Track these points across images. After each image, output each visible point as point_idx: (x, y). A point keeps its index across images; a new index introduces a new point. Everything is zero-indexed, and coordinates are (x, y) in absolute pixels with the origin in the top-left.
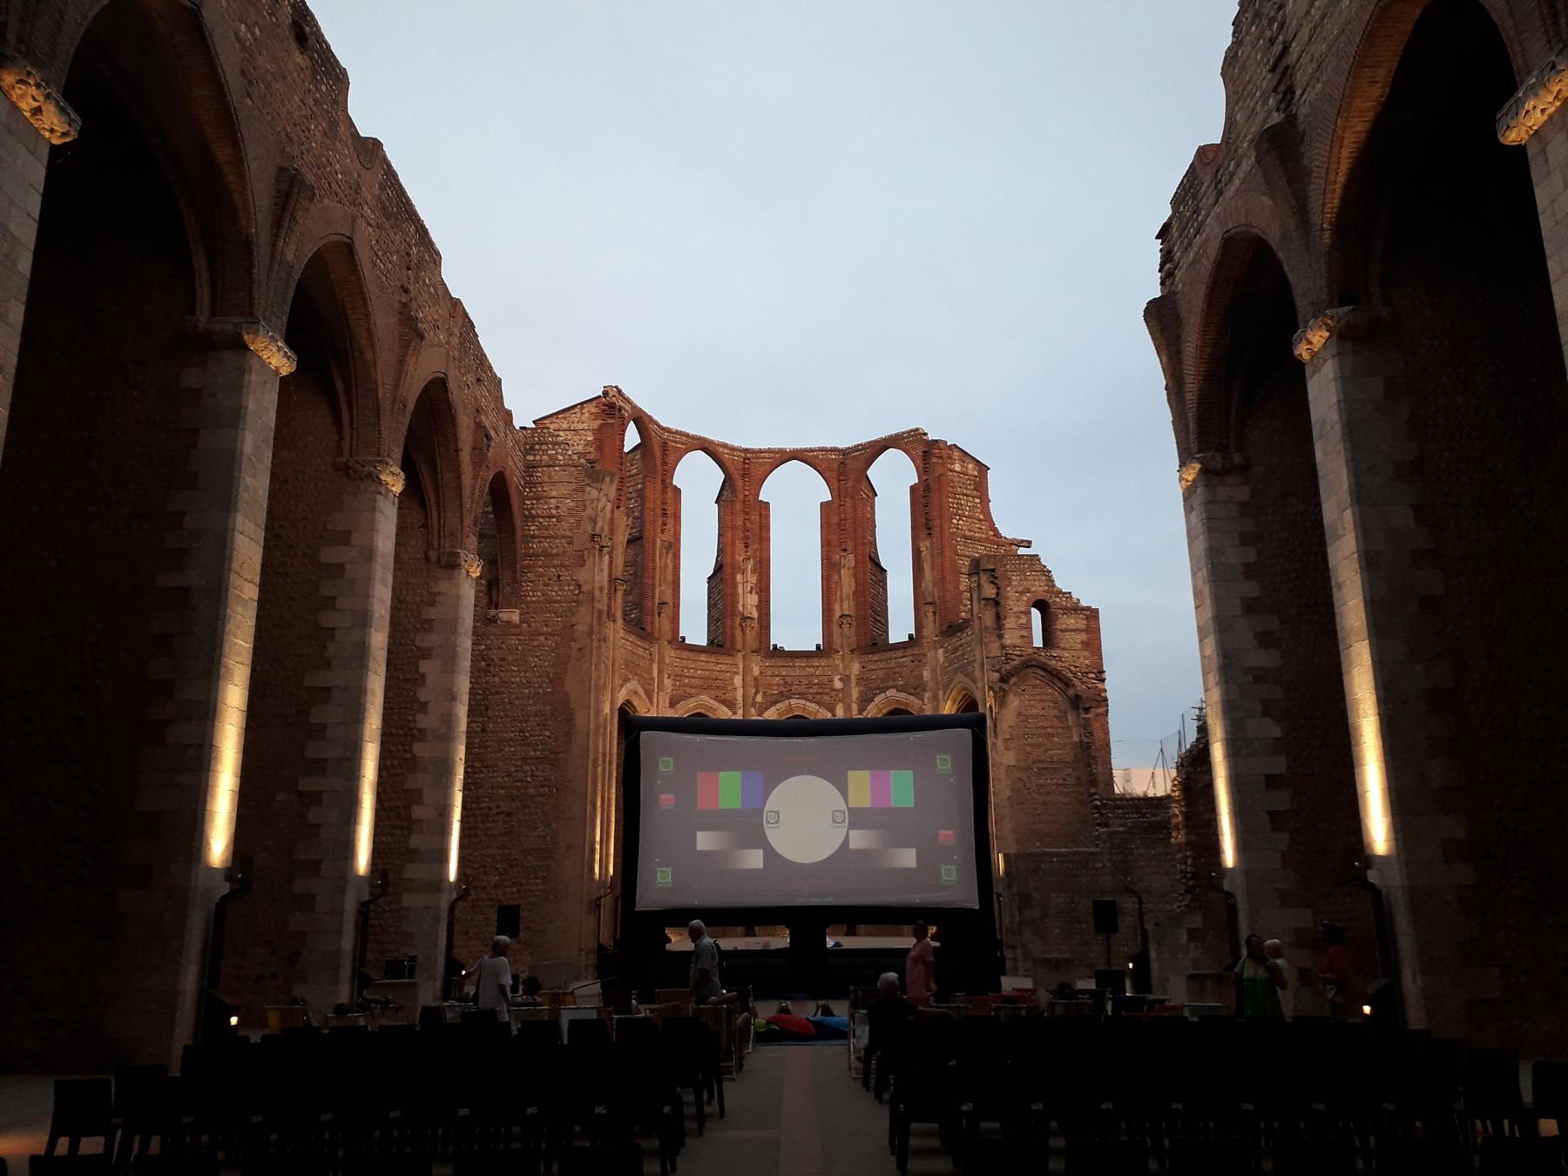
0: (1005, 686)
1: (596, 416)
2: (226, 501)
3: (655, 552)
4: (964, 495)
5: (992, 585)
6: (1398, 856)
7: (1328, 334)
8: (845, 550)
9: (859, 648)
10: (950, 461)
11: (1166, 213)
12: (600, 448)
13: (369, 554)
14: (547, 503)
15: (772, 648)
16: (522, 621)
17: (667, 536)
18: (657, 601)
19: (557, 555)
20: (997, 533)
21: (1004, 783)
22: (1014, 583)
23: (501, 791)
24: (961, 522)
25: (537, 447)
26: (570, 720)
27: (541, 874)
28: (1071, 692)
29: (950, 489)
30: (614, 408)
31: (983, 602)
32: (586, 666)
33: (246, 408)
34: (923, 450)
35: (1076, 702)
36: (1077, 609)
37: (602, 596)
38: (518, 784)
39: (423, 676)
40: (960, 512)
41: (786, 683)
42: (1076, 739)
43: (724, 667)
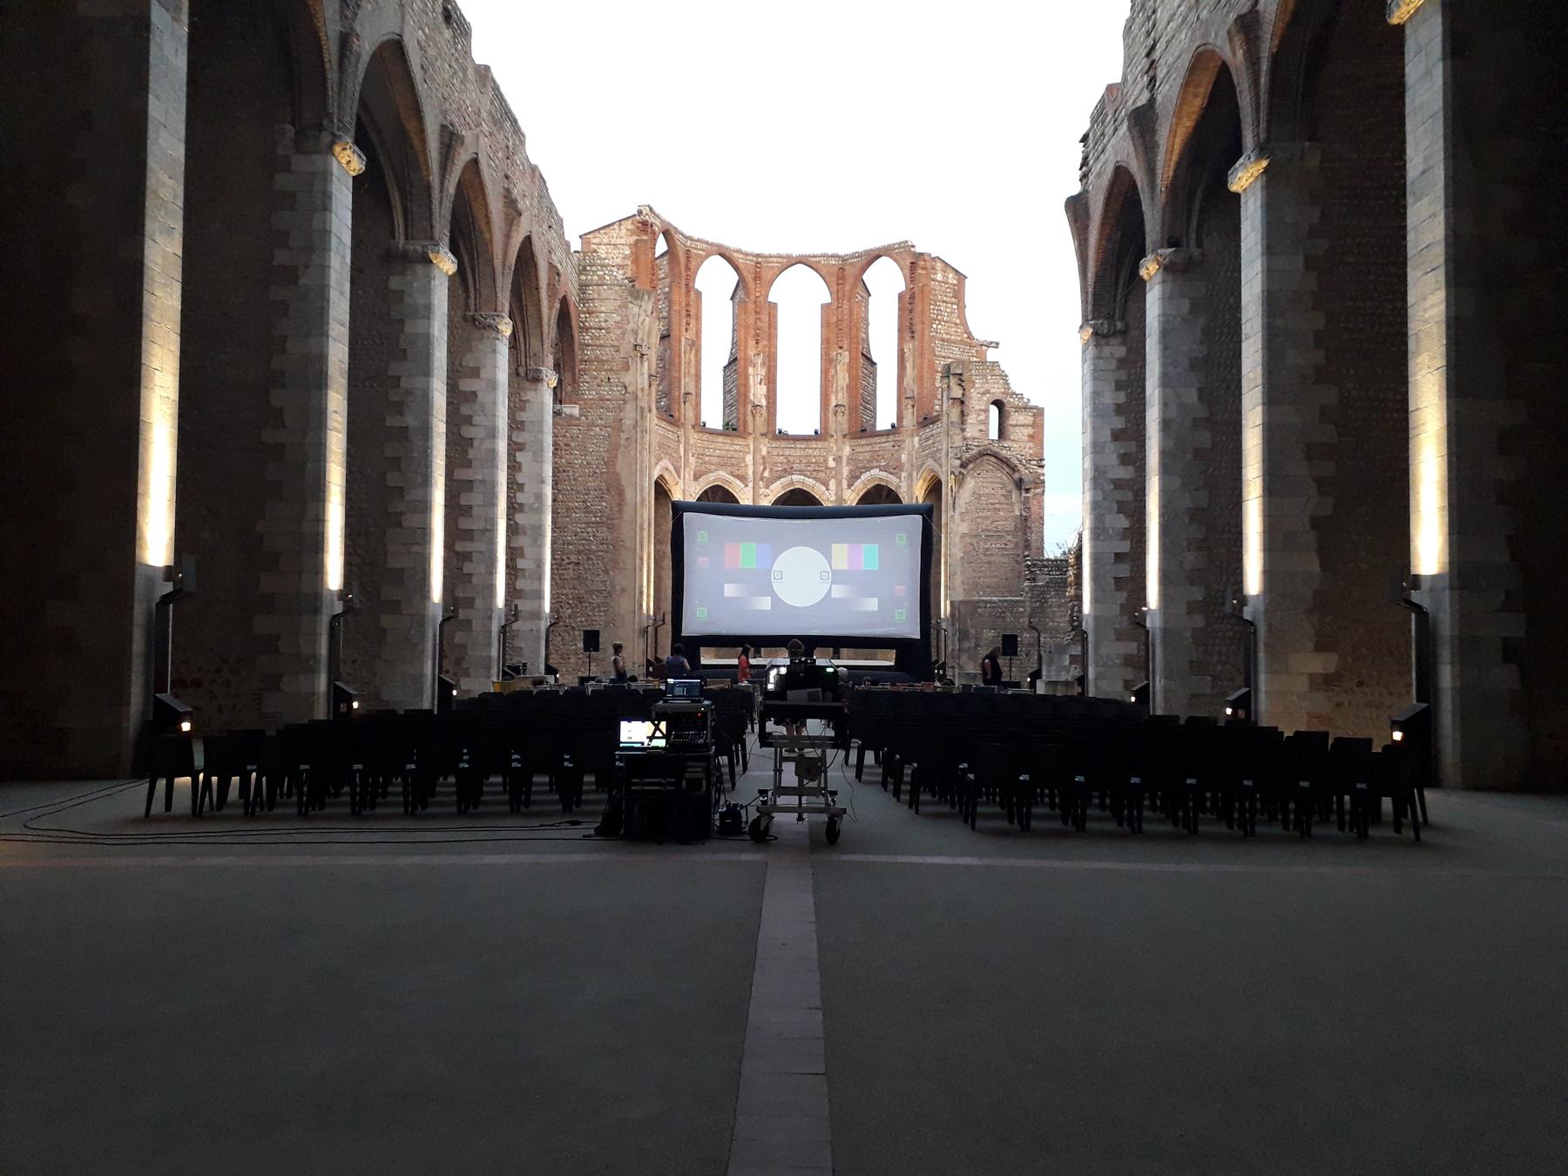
0: (963, 471)
1: (632, 233)
2: (427, 372)
3: (680, 350)
4: (944, 302)
5: (959, 387)
6: (1160, 609)
7: (1157, 267)
8: (841, 348)
9: (850, 433)
10: (933, 271)
11: (1085, 126)
12: (636, 261)
13: (493, 385)
14: (597, 316)
15: (777, 431)
16: (581, 415)
17: (691, 335)
18: (683, 391)
19: (607, 361)
20: (970, 336)
21: (957, 547)
22: (977, 386)
23: (570, 547)
24: (940, 326)
25: (588, 268)
26: (621, 494)
27: (603, 609)
28: (1016, 476)
29: (932, 297)
30: (647, 225)
31: (951, 401)
32: (632, 453)
33: (434, 305)
34: (910, 261)
35: (1019, 484)
36: (1026, 408)
37: (643, 396)
38: (583, 542)
39: (520, 464)
40: (939, 317)
41: (789, 461)
42: (1017, 513)
43: (738, 448)
